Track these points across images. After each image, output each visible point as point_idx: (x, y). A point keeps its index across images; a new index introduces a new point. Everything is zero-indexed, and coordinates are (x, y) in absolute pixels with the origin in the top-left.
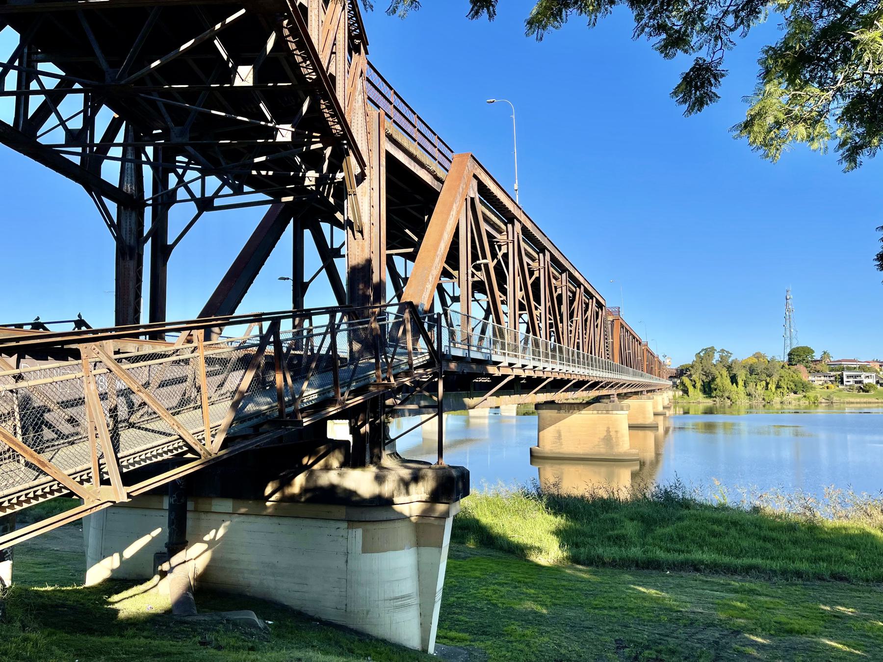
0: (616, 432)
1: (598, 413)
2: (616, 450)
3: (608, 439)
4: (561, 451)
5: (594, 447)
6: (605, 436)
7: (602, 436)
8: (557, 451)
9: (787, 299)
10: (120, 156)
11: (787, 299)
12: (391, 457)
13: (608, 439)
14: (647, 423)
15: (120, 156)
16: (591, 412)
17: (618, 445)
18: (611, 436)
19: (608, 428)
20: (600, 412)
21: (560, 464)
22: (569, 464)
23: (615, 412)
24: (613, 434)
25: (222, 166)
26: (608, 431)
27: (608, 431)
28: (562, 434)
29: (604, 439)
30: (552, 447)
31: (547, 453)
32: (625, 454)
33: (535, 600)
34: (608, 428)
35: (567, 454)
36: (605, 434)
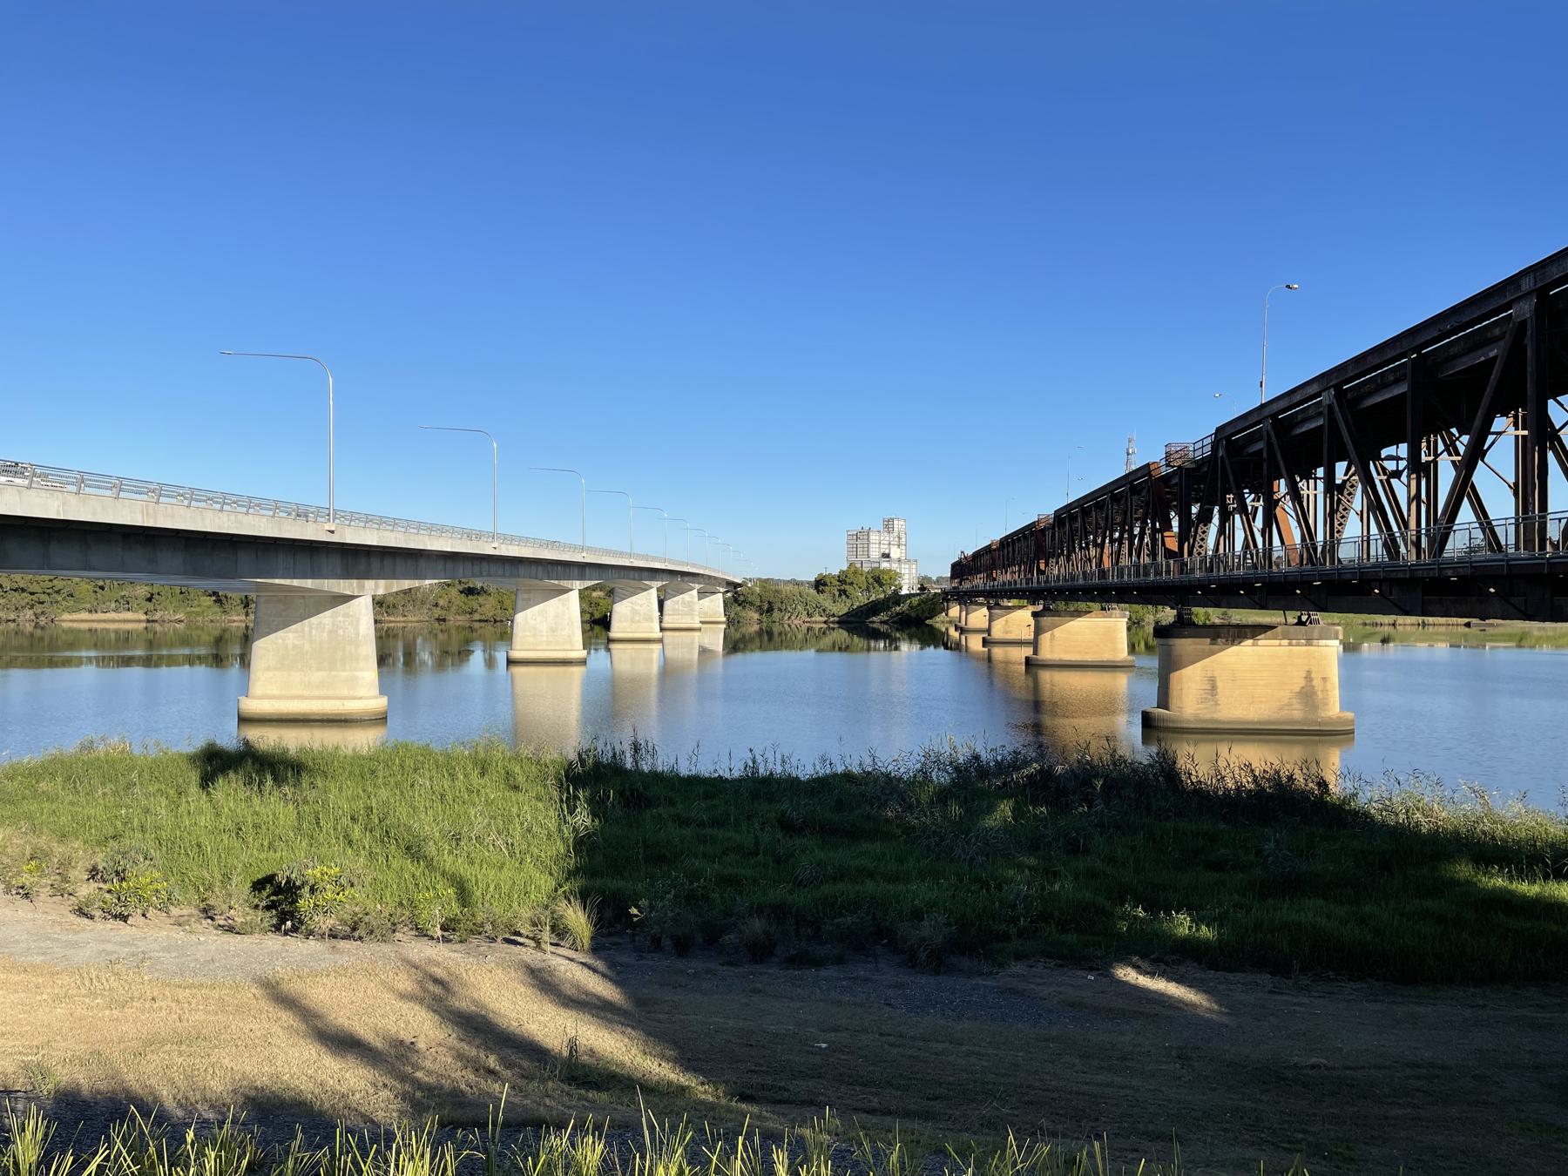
0: (1324, 679)
1: (1290, 645)
2: (1323, 715)
3: (1308, 695)
4: (1217, 716)
5: (1281, 709)
6: (1303, 688)
7: (1297, 689)
8: (1208, 716)
9: (1128, 454)
10: (1395, 462)
11: (1128, 454)
12: (383, 713)
13: (1308, 695)
14: (1118, 659)
15: (1395, 462)
16: (1277, 642)
17: (1326, 704)
18: (1313, 687)
19: (1309, 672)
20: (1294, 641)
21: (1213, 741)
22: (297, 714)
23: (1323, 642)
24: (1317, 683)
25: (1262, 450)
26: (1308, 678)
27: (1308, 678)
28: (1219, 684)
29: (1300, 693)
30: (1199, 709)
31: (1188, 721)
32: (1331, 721)
33: (1102, 1148)
34: (1309, 672)
35: (1228, 722)
36: (1302, 683)
